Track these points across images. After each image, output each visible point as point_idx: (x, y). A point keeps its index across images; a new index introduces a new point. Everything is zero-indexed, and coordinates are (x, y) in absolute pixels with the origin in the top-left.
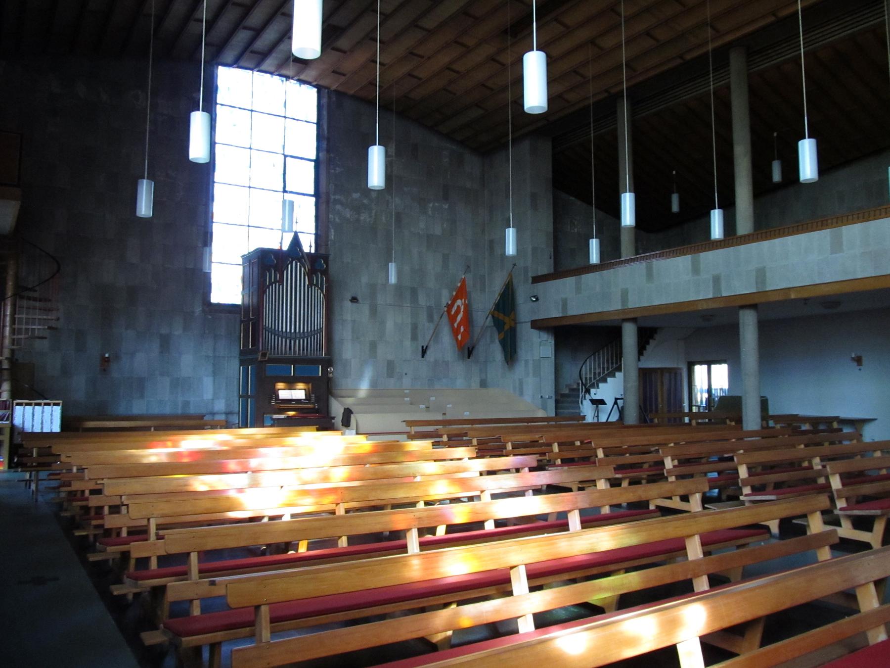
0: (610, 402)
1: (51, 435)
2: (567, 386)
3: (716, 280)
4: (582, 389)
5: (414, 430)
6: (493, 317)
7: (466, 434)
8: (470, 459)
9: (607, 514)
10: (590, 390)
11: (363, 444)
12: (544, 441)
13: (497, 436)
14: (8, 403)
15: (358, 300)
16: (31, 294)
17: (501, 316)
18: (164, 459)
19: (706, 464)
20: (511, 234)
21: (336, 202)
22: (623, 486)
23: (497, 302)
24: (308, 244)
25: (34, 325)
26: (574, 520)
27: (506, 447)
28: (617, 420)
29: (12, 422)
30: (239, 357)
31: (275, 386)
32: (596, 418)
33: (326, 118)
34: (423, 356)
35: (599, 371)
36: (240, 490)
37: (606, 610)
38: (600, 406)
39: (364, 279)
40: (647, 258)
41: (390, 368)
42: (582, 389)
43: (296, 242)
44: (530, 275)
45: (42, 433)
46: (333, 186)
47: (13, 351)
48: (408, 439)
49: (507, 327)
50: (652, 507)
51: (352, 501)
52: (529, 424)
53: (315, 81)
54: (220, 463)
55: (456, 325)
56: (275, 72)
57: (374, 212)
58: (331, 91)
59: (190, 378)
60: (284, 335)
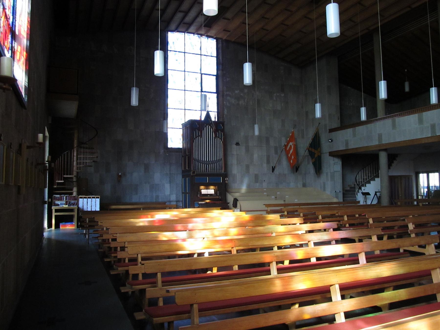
0: (372, 194)
1: (96, 212)
2: (349, 186)
3: (433, 127)
4: (357, 187)
5: (269, 209)
6: (309, 151)
7: (297, 211)
8: (300, 224)
9: (378, 254)
10: (361, 188)
11: (245, 216)
12: (339, 214)
13: (314, 212)
14: (76, 197)
15: (239, 144)
16: (85, 146)
17: (313, 150)
18: (146, 224)
19: (430, 227)
20: (318, 106)
21: (227, 95)
22: (384, 239)
23: (310, 143)
24: (214, 117)
25: (87, 160)
26: (362, 258)
27: (318, 217)
28: (376, 203)
29: (78, 206)
30: (182, 174)
31: (199, 188)
32: (365, 203)
33: (221, 54)
34: (273, 172)
35: (366, 177)
36: (184, 240)
37: (383, 309)
38: (367, 196)
39: (242, 134)
40: (392, 117)
41: (256, 178)
42: (357, 187)
43: (208, 116)
44: (328, 128)
45: (91, 211)
46: (226, 88)
47: (78, 173)
48: (267, 213)
49: (316, 156)
50: (401, 251)
51: (240, 246)
52: (330, 205)
53: (215, 36)
54: (174, 226)
55: (289, 155)
56: (195, 33)
57: (246, 99)
58: (223, 40)
59: (158, 184)
60: (203, 162)
